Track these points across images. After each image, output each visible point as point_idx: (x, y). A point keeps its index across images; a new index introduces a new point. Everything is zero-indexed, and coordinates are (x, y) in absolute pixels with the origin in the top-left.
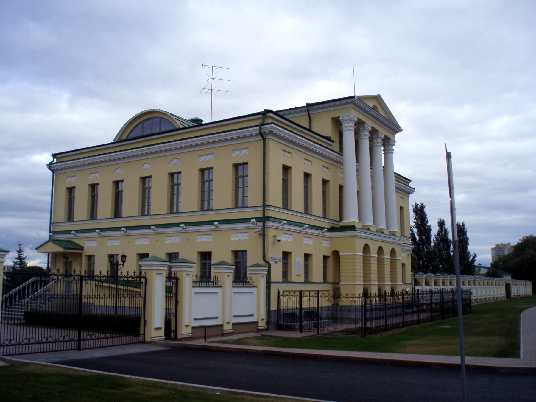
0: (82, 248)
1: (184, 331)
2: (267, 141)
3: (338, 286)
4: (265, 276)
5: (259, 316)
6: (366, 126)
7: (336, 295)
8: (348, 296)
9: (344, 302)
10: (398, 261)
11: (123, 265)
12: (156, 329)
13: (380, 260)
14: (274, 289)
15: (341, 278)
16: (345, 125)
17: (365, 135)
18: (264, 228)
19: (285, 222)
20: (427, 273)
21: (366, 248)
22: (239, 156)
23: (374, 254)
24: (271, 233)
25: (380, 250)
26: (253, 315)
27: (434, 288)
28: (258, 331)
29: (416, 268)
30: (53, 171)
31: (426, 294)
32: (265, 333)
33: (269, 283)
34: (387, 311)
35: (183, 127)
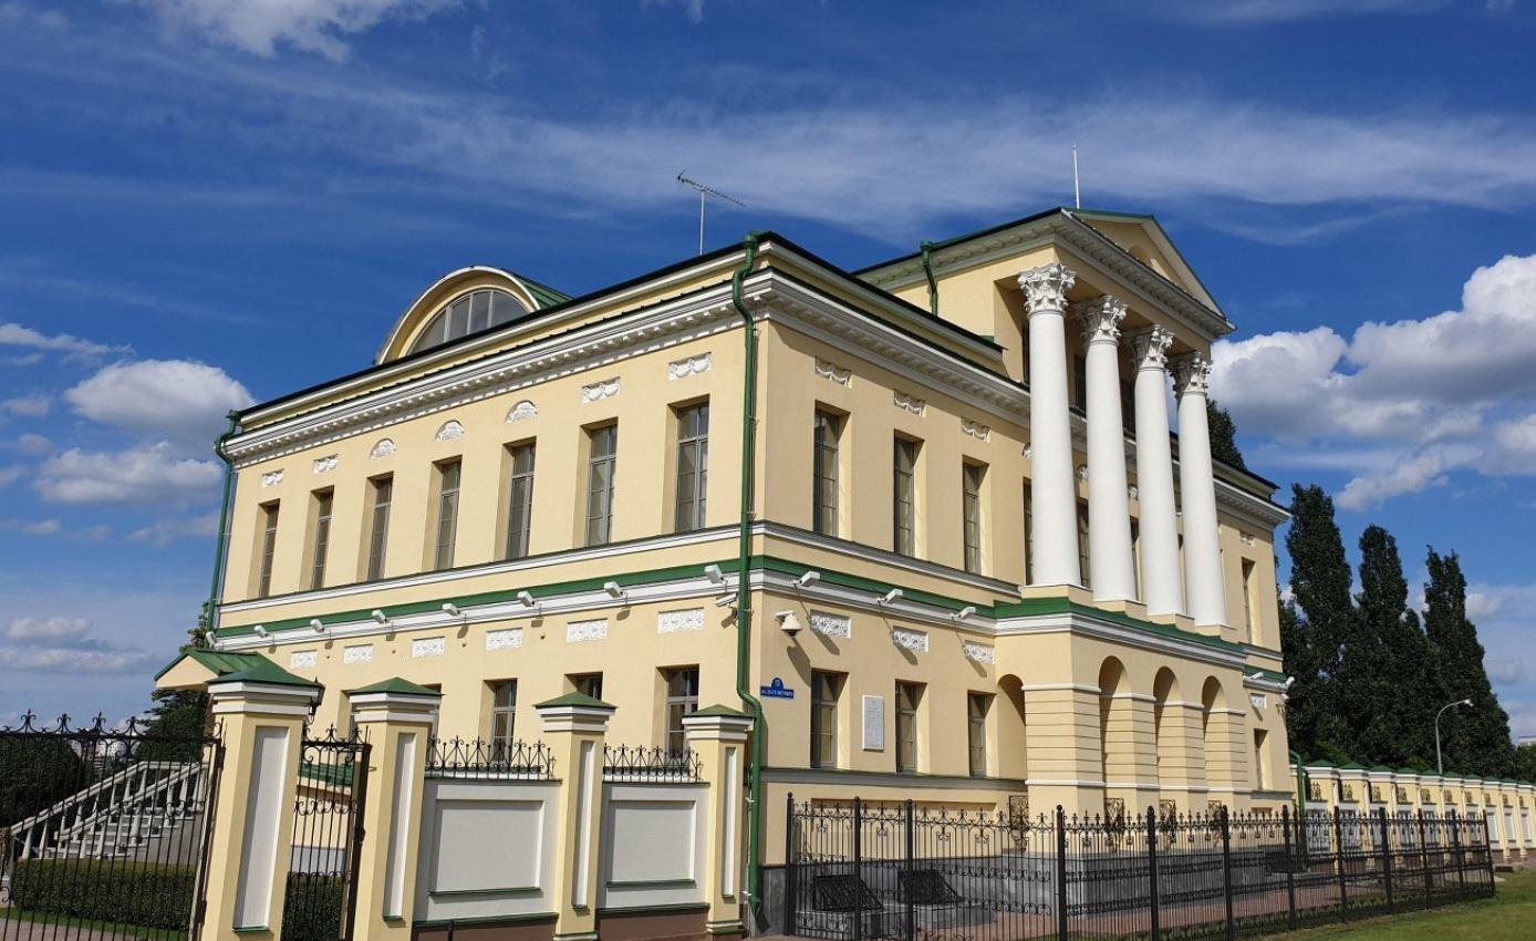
11: (313, 714)
14: (776, 794)
16: (1034, 296)
35: (555, 304)
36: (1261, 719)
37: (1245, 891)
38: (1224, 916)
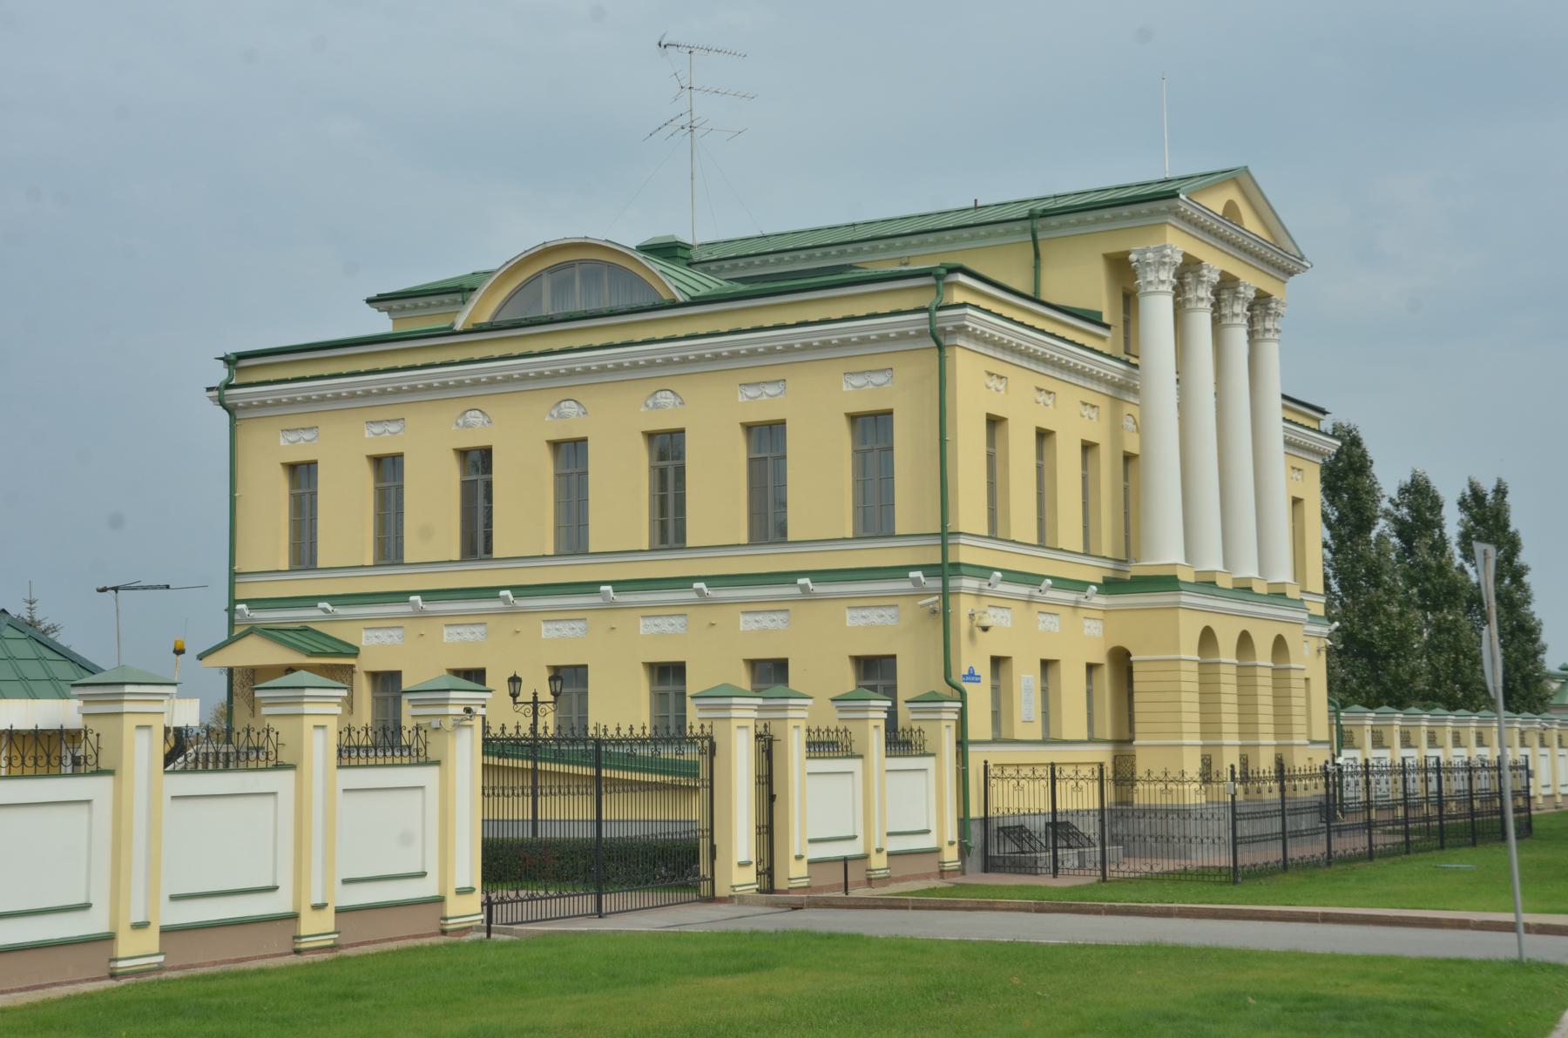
0: (354, 652)
1: (793, 872)
2: (948, 353)
3: (1126, 749)
4: (953, 724)
5: (943, 835)
6: (1205, 272)
7: (1123, 775)
8: (1153, 776)
9: (1144, 795)
10: (1293, 674)
12: (741, 865)
13: (1246, 673)
15: (1138, 728)
17: (1202, 299)
18: (945, 593)
19: (999, 574)
20: (1380, 705)
21: (1208, 638)
22: (862, 393)
23: (1227, 652)
24: (964, 606)
25: (1245, 640)
26: (927, 832)
27: (1414, 756)
28: (942, 873)
29: (1343, 692)
30: (231, 410)
31: (1311, 777)
32: (960, 880)
33: (962, 744)
34: (1288, 819)
36: (200, 657)
37: (1298, 834)
38: (1280, 856)
